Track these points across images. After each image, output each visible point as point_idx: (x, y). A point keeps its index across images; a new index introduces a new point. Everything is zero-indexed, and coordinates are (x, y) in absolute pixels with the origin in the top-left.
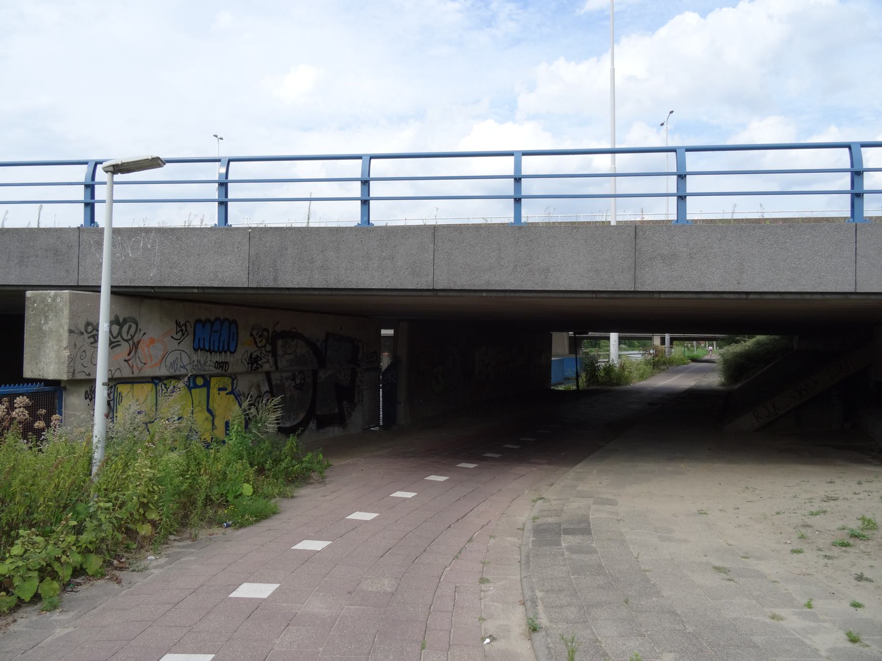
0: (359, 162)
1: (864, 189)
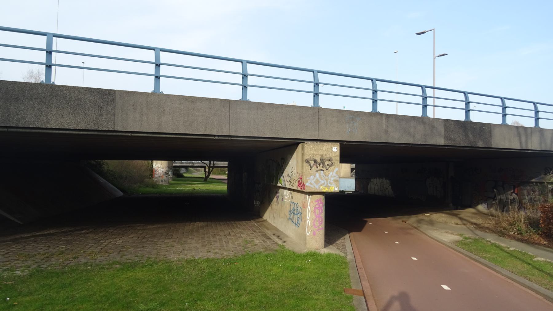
0: (45, 38)
1: (248, 84)
